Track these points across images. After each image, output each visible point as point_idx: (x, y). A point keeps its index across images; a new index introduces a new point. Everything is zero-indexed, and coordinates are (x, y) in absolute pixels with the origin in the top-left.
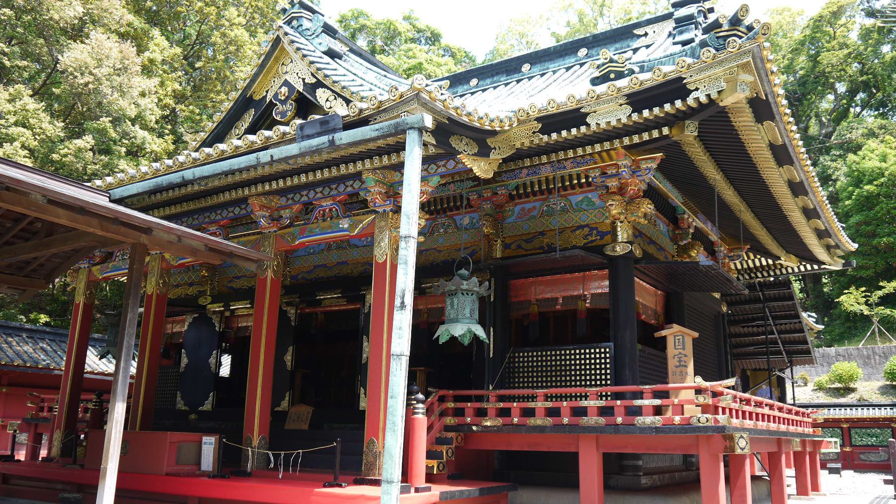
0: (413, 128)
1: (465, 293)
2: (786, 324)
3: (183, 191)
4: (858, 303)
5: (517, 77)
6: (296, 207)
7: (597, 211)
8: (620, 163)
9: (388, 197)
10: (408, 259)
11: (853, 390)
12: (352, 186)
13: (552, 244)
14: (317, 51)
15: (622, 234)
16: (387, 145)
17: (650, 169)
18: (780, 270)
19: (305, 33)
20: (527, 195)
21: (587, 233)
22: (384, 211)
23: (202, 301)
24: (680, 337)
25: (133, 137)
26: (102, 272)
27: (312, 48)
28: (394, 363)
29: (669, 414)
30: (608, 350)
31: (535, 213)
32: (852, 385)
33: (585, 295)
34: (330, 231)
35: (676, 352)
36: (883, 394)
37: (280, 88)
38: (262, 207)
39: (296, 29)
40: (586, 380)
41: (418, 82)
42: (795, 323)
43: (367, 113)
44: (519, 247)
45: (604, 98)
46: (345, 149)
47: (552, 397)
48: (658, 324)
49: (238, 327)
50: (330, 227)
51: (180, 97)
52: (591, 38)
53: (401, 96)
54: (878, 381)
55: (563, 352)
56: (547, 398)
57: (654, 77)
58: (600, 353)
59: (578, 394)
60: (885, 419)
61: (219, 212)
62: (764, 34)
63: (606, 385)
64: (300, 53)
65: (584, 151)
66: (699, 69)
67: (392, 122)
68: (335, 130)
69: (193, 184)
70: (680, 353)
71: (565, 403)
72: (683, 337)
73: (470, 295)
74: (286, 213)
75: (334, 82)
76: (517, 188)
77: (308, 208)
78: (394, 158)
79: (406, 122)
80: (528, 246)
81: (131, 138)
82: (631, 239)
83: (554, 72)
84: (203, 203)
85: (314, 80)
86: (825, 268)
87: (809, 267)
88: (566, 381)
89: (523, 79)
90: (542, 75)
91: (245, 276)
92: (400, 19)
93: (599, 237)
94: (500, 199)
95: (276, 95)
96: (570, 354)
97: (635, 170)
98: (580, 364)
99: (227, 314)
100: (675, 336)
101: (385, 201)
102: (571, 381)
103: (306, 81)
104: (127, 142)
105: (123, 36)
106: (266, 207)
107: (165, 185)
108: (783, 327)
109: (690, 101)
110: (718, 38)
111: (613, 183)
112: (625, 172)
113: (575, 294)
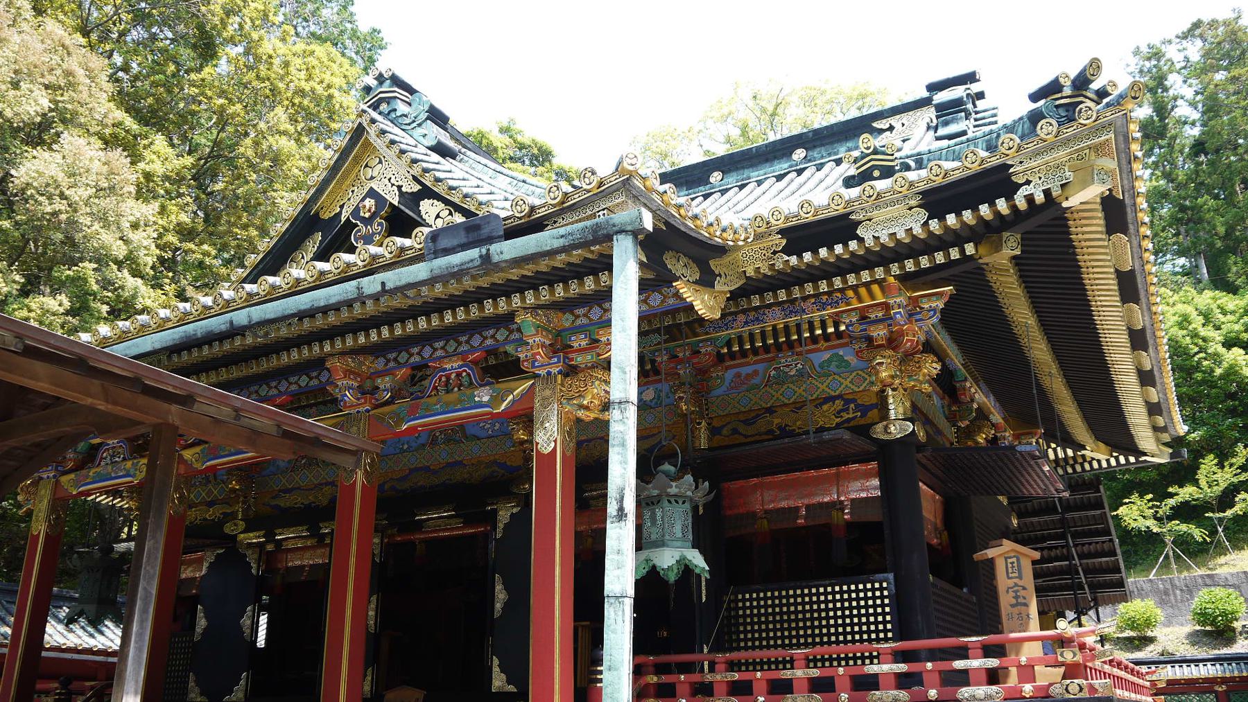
0: (623, 231)
1: (672, 500)
2: (1090, 544)
3: (227, 346)
4: (1144, 517)
5: (703, 190)
6: (402, 373)
7: (854, 374)
8: (892, 302)
9: (554, 352)
10: (627, 437)
11: (1151, 640)
12: (493, 336)
13: (786, 425)
14: (419, 145)
15: (896, 408)
16: (569, 264)
17: (935, 310)
18: (1082, 465)
19: (400, 120)
20: (743, 353)
21: (840, 407)
22: (549, 373)
23: (228, 529)
24: (1014, 560)
25: (119, 287)
26: (77, 484)
27: (413, 142)
28: (612, 610)
29: (1013, 680)
30: (885, 585)
31: (756, 380)
32: (1149, 634)
33: (842, 502)
34: (459, 406)
35: (1010, 583)
36: (1193, 644)
37: (363, 200)
38: (348, 373)
39: (386, 116)
40: (853, 633)
41: (630, 161)
42: (1103, 542)
43: (542, 212)
44: (735, 431)
45: (888, 197)
46: (502, 270)
47: (815, 660)
48: (940, 544)
49: (287, 568)
50: (460, 401)
51: (186, 233)
52: (811, 134)
53: (601, 184)
54: (1182, 625)
55: (814, 590)
56: (810, 662)
57: (896, 187)
58: (873, 590)
59: (819, 657)
60: (1206, 680)
61: (274, 384)
62: (1135, 98)
63: (886, 640)
64: (396, 148)
65: (845, 281)
66: (1033, 151)
67: (588, 223)
68: (490, 240)
69: (244, 335)
70: (1016, 585)
71: (841, 669)
72: (1018, 560)
73: (680, 502)
74: (384, 383)
75: (451, 188)
76: (729, 344)
77: (419, 373)
78: (574, 286)
79: (611, 222)
80: (750, 431)
81: (116, 290)
82: (909, 415)
83: (759, 183)
84: (265, 365)
85: (417, 188)
86: (1145, 461)
87: (1122, 460)
88: (813, 636)
89: (712, 193)
90: (742, 187)
91: (299, 488)
92: (496, 131)
93: (859, 414)
94: (705, 360)
95: (357, 210)
96: (795, 596)
97: (913, 312)
98: (759, 615)
99: (270, 547)
100: (1006, 559)
101: (550, 358)
102: (829, 635)
103: (404, 189)
104: (110, 294)
105: (109, 142)
106: (354, 373)
107: (199, 335)
108: (1086, 548)
109: (1020, 201)
110: (1057, 107)
111: (879, 332)
112: (899, 314)
113: (825, 500)
